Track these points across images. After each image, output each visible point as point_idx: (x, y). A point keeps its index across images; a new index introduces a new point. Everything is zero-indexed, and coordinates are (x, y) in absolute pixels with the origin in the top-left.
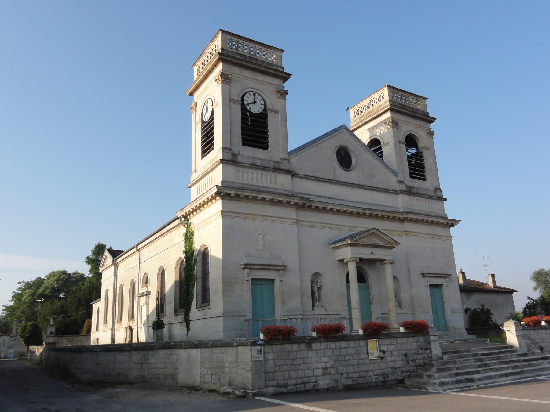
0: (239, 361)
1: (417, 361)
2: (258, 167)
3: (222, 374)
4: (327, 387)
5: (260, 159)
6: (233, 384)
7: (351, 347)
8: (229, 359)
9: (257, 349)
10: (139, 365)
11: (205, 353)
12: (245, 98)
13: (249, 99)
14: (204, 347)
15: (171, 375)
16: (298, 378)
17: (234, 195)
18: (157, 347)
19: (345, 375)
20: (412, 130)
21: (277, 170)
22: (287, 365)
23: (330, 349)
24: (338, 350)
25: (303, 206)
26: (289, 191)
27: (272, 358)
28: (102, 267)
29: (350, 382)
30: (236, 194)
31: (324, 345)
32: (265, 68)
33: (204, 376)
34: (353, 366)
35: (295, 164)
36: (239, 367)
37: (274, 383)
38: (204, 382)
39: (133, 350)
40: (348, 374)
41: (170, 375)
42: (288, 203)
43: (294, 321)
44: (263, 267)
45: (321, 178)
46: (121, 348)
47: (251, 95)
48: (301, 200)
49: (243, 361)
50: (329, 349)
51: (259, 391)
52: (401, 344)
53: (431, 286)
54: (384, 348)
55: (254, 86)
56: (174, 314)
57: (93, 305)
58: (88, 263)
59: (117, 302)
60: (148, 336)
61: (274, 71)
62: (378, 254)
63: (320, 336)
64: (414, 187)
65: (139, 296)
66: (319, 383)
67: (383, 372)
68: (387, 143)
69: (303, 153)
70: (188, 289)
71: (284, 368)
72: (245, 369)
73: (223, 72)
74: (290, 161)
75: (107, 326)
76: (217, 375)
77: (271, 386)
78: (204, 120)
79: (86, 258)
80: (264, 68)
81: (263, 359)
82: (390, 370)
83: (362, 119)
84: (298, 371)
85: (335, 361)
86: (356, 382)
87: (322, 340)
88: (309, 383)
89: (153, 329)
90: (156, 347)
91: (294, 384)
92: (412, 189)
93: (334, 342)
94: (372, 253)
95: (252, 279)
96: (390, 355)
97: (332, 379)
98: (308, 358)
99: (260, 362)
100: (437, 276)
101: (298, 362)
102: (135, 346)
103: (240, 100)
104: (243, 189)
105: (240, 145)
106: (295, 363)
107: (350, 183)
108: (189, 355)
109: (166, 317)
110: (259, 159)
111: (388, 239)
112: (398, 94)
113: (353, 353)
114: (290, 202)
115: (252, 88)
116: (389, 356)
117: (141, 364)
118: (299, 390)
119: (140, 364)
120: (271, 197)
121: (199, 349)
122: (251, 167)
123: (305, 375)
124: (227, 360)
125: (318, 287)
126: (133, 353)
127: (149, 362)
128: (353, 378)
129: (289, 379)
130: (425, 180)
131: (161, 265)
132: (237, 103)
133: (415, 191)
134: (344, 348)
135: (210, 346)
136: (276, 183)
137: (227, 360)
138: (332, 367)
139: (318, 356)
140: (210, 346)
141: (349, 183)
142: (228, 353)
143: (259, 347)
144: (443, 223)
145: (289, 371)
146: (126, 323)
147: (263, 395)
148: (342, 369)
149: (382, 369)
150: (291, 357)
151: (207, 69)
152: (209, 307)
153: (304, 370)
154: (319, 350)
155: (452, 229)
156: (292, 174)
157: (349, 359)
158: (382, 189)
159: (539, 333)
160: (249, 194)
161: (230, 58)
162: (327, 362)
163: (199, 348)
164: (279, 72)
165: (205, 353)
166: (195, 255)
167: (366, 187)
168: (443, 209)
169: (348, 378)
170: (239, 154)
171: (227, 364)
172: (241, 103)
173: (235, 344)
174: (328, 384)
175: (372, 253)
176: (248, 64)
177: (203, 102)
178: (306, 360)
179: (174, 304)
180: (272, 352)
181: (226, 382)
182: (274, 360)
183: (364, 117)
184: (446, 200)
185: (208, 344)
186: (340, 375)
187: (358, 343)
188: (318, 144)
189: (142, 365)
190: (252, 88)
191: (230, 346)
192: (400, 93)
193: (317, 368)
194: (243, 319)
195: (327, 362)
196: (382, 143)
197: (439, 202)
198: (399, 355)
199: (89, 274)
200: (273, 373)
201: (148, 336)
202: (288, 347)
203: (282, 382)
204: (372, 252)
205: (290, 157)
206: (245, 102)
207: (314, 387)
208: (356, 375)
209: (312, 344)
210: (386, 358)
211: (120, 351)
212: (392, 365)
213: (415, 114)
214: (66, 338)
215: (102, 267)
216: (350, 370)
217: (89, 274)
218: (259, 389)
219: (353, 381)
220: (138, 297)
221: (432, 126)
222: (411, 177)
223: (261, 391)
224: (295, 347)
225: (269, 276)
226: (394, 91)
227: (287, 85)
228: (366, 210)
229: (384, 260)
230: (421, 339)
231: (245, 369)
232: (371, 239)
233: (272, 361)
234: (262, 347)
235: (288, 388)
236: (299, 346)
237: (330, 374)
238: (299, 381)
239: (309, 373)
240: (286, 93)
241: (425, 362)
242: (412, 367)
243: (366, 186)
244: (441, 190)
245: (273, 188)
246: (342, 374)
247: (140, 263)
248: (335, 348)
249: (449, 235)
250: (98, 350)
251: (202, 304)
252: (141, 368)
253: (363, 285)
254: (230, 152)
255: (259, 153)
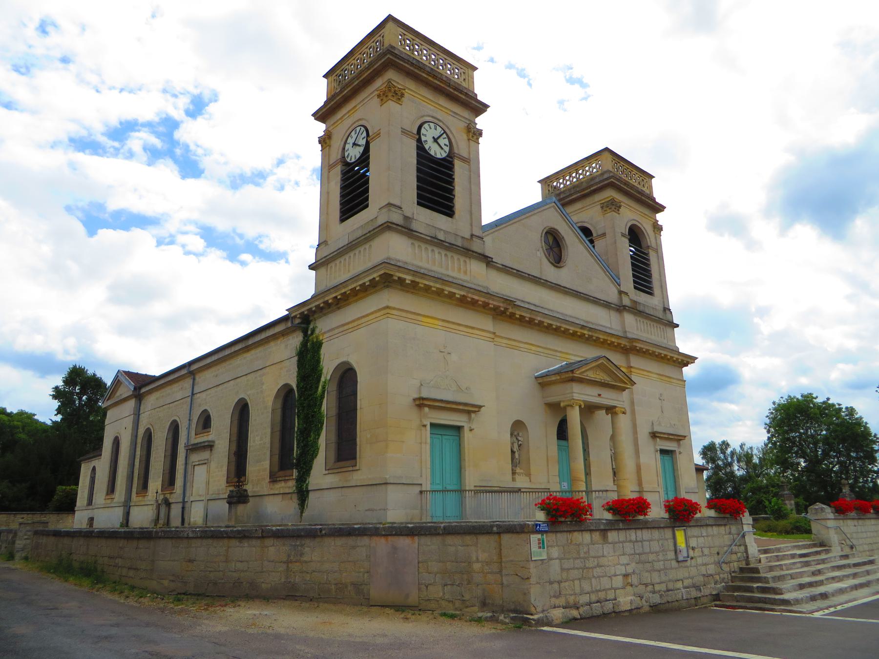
0: (503, 560)
1: (730, 564)
2: (442, 242)
3: (467, 584)
4: (630, 608)
5: (444, 231)
6: (490, 602)
7: (655, 540)
8: (483, 556)
9: (538, 539)
10: (284, 566)
11: (430, 546)
12: (423, 131)
13: (429, 134)
14: (428, 534)
15: (353, 584)
16: (593, 592)
17: (410, 282)
18: (324, 532)
19: (650, 588)
20: (637, 219)
21: (467, 252)
22: (577, 569)
23: (630, 541)
24: (640, 544)
25: (503, 313)
26: (484, 287)
27: (557, 556)
28: (107, 400)
29: (656, 599)
30: (412, 281)
31: (622, 535)
32: (453, 89)
33: (427, 587)
34: (659, 571)
35: (490, 247)
36: (504, 572)
37: (562, 601)
38: (427, 598)
39: (269, 537)
40: (653, 585)
41: (353, 584)
42: (485, 305)
43: (525, 496)
44: (448, 406)
45: (526, 273)
46: (144, 535)
47: (430, 128)
48: (503, 302)
49: (512, 561)
50: (628, 542)
51: (543, 617)
52: (713, 536)
53: (663, 452)
54: (693, 543)
55: (435, 115)
56: (268, 480)
57: (82, 462)
58: (55, 397)
59: (136, 459)
60: (207, 516)
61: (465, 96)
62: (608, 398)
63: (617, 519)
64: (640, 303)
65: (190, 449)
66: (619, 601)
67: (694, 582)
68: (604, 235)
69: (501, 231)
70: (307, 438)
71: (575, 574)
72: (517, 575)
73: (317, 117)
74: (484, 240)
75: (113, 497)
76: (455, 586)
77: (558, 607)
78: (348, 160)
79: (53, 388)
80: (451, 88)
81: (546, 558)
82: (702, 579)
83: (562, 197)
84: (591, 579)
85: (637, 563)
86: (664, 600)
87: (621, 525)
88: (607, 600)
89: (228, 503)
90: (321, 532)
91: (588, 603)
92: (638, 306)
93: (634, 531)
94: (600, 395)
95: (432, 425)
96: (701, 554)
97: (634, 595)
98: (603, 556)
99: (542, 564)
100: (670, 437)
101: (591, 563)
102: (442, 525)
103: (415, 132)
104: (424, 275)
105: (414, 203)
106: (587, 565)
107: (562, 285)
108: (395, 548)
109: (249, 484)
110: (442, 230)
111: (621, 375)
112: (619, 164)
113: (657, 549)
114: (489, 304)
115: (432, 117)
116: (700, 556)
117: (288, 562)
118: (595, 613)
119: (284, 562)
120: (462, 293)
121: (416, 538)
122: (431, 241)
123: (600, 588)
124: (477, 559)
125: (519, 443)
126: (269, 542)
127: (305, 558)
128: (659, 591)
129: (580, 595)
130: (651, 294)
131: (241, 397)
132: (411, 136)
133: (641, 308)
134: (647, 541)
135: (441, 533)
136: (465, 273)
137: (477, 559)
138: (634, 573)
139: (616, 554)
140: (441, 533)
141: (560, 286)
142: (479, 545)
143: (539, 536)
144: (677, 359)
145: (579, 579)
146: (157, 493)
147: (550, 624)
148: (647, 577)
149: (692, 578)
150: (582, 555)
151: (360, 77)
152: (354, 468)
153: (599, 577)
154: (616, 543)
155: (685, 369)
156: (487, 260)
157: (653, 560)
158: (601, 300)
159: (849, 525)
160: (431, 284)
161: (405, 62)
162: (628, 564)
163: (416, 535)
164: (472, 99)
165: (430, 546)
166: (323, 379)
167: (581, 295)
168: (673, 340)
169: (654, 592)
170: (413, 219)
171: (477, 566)
172: (418, 137)
173: (495, 529)
174: (631, 603)
175: (600, 395)
176: (430, 78)
177: (346, 132)
178: (603, 561)
179: (268, 462)
180: (557, 546)
181: (476, 599)
182: (560, 559)
183: (565, 194)
184: (677, 326)
185: (436, 528)
186: (643, 587)
187: (663, 533)
188: (521, 220)
189: (290, 565)
190: (432, 117)
191: (484, 533)
192: (621, 162)
193: (615, 575)
194: (418, 489)
195: (628, 564)
196: (594, 235)
197: (669, 330)
198: (711, 555)
199: (56, 415)
200: (559, 582)
201: (207, 516)
202: (577, 537)
203: (571, 599)
204: (599, 393)
205: (483, 235)
206: (422, 137)
207: (613, 607)
208: (663, 587)
209: (607, 533)
210: (696, 559)
211: (240, 538)
212: (703, 570)
213: (642, 195)
214: (22, 516)
215: (107, 400)
216: (656, 577)
217: (56, 415)
218: (543, 611)
219: (661, 596)
220: (187, 450)
221: (659, 216)
222: (635, 288)
223: (546, 616)
224: (587, 536)
225: (453, 420)
226: (614, 158)
227: (481, 122)
228: (584, 329)
229: (615, 407)
230: (734, 529)
231: (517, 575)
232: (598, 373)
233: (558, 560)
234: (545, 535)
235: (581, 610)
236: (591, 535)
237: (632, 585)
238: (594, 598)
239: (605, 583)
240: (480, 133)
241: (741, 566)
242: (726, 575)
243: (582, 293)
244: (671, 312)
245: (461, 280)
246: (646, 585)
247: (193, 394)
248: (637, 541)
249: (682, 379)
250: (191, 535)
251: (335, 462)
252: (288, 570)
253: (563, 443)
254: (400, 212)
255: (440, 221)
